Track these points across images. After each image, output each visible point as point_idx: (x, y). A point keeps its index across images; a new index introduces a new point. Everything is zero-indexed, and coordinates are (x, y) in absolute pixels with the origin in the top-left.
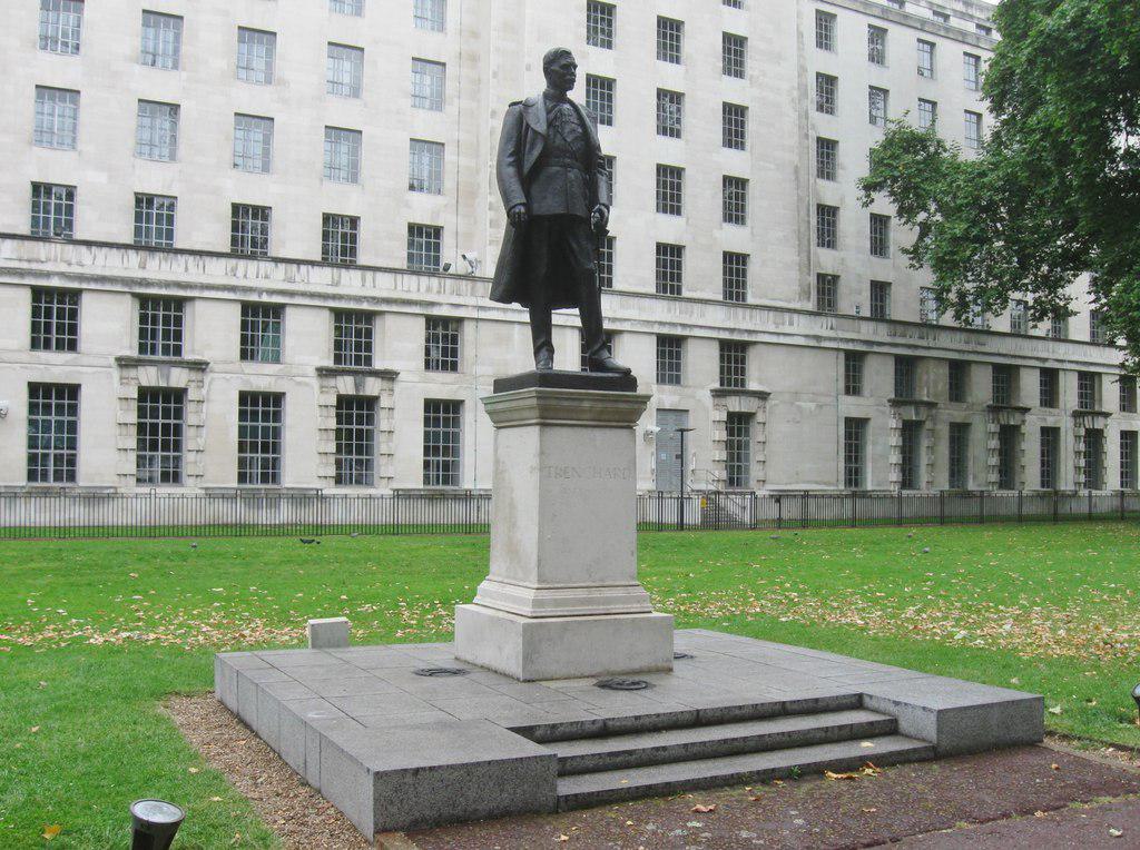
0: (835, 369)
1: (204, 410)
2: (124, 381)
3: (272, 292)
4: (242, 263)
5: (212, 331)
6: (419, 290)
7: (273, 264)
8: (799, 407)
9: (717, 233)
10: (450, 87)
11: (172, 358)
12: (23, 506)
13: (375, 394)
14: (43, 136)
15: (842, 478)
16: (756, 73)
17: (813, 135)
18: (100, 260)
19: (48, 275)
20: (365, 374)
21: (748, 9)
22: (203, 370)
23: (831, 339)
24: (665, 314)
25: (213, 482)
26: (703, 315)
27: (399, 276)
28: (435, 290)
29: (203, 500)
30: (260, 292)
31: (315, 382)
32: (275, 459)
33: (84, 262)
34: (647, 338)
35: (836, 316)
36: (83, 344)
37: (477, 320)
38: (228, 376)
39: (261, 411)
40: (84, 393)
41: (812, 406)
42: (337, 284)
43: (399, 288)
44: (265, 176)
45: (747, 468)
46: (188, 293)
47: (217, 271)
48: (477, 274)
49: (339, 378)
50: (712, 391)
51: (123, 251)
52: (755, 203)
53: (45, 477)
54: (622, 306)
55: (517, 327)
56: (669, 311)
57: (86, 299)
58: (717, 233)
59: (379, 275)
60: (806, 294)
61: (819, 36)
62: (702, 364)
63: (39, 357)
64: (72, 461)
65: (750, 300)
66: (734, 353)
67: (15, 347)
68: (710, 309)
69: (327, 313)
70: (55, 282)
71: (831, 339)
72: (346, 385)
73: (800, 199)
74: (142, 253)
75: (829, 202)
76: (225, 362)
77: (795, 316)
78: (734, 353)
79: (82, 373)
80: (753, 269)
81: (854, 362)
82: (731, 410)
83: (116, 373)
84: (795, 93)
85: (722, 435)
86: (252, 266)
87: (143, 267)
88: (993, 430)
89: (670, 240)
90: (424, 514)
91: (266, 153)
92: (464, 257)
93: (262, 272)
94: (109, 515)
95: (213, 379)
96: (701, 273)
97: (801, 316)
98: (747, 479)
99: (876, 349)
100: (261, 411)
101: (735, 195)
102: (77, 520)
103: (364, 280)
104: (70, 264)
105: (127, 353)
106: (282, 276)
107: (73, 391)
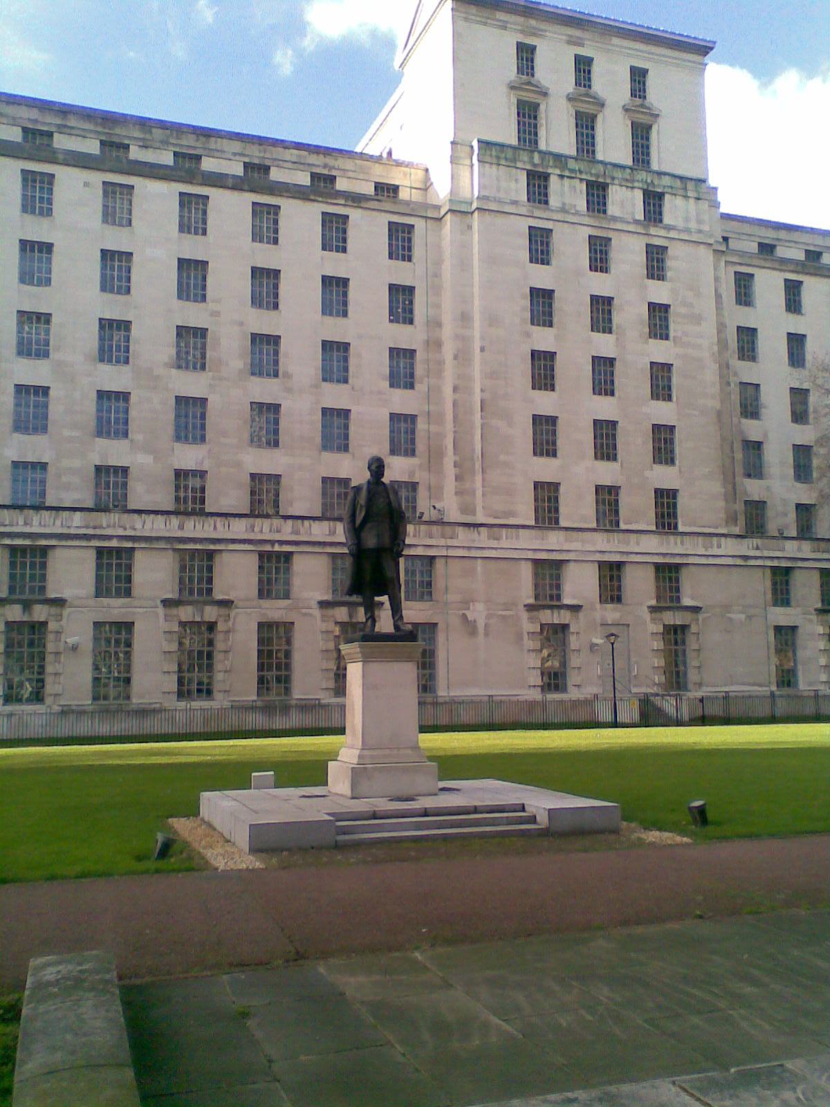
0: (761, 585)
3: (281, 543)
4: (258, 521)
5: (236, 575)
8: (730, 619)
9: (647, 473)
10: (419, 370)
11: (675, 604)
13: (567, 622)
14: (21, 426)
15: (774, 679)
16: (679, 334)
17: (734, 381)
18: (148, 525)
19: (110, 538)
20: (205, 603)
21: (671, 280)
23: (756, 558)
24: (607, 546)
26: (719, 546)
29: (33, 717)
30: (272, 542)
31: (317, 612)
34: (590, 565)
35: (768, 537)
36: (136, 591)
39: (116, 638)
40: (137, 628)
41: (743, 617)
44: (276, 450)
45: (685, 674)
46: (218, 547)
47: (239, 528)
48: (445, 520)
49: (8, 607)
50: (649, 607)
51: (165, 516)
52: (681, 447)
54: (566, 540)
55: (479, 561)
56: (608, 541)
57: (139, 557)
58: (647, 473)
60: (732, 519)
61: (738, 295)
62: (640, 586)
65: (681, 528)
66: (668, 574)
68: (644, 537)
70: (114, 543)
71: (756, 558)
72: (186, 613)
73: (723, 439)
74: (180, 517)
75: (754, 437)
77: (723, 539)
78: (668, 574)
80: (682, 502)
81: (781, 578)
82: (667, 623)
83: (161, 611)
84: (716, 348)
85: (658, 644)
86: (266, 524)
87: (181, 527)
88: (822, 632)
89: (607, 482)
92: (434, 507)
93: (274, 527)
96: (637, 508)
97: (729, 539)
98: (686, 683)
99: (800, 564)
100: (116, 638)
101: (663, 443)
104: (125, 529)
105: (169, 596)
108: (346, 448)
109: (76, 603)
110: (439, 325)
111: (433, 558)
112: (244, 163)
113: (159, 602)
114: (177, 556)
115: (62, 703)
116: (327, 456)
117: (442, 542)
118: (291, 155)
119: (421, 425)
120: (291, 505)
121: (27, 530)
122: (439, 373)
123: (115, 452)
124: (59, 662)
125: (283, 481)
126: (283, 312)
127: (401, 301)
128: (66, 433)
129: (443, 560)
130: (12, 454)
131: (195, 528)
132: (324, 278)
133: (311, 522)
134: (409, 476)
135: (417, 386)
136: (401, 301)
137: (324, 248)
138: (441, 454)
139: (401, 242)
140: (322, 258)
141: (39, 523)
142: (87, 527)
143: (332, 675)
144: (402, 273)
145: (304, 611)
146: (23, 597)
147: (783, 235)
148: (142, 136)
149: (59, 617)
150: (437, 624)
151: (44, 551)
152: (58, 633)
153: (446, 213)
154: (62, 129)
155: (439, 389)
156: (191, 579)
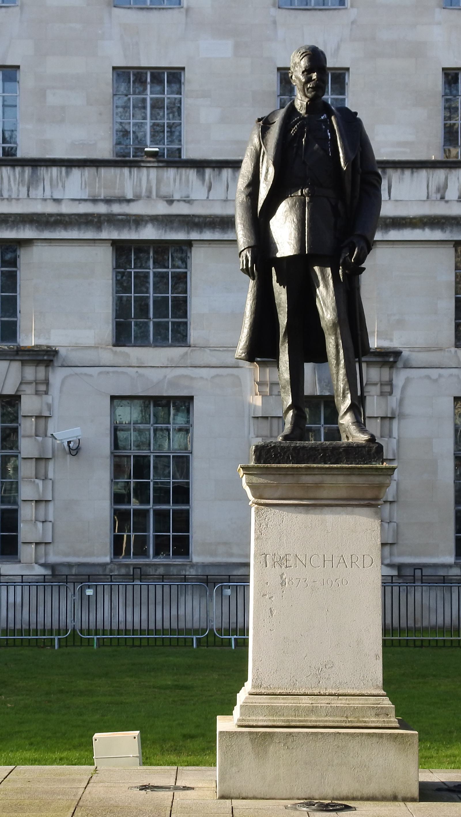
1: (395, 434)
19: (138, 221)
25: (411, 555)
33: (193, 197)
36: (194, 334)
38: (434, 373)
53: (141, 550)
63: (127, 355)
64: (183, 521)
67: (91, 342)
70: (149, 233)
76: (428, 349)
79: (192, 378)
95: (408, 380)
102: (189, 618)
104: (170, 202)
107: (185, 403)
109: (75, 357)
115: (53, 559)
142: (94, 201)
149: (43, 387)
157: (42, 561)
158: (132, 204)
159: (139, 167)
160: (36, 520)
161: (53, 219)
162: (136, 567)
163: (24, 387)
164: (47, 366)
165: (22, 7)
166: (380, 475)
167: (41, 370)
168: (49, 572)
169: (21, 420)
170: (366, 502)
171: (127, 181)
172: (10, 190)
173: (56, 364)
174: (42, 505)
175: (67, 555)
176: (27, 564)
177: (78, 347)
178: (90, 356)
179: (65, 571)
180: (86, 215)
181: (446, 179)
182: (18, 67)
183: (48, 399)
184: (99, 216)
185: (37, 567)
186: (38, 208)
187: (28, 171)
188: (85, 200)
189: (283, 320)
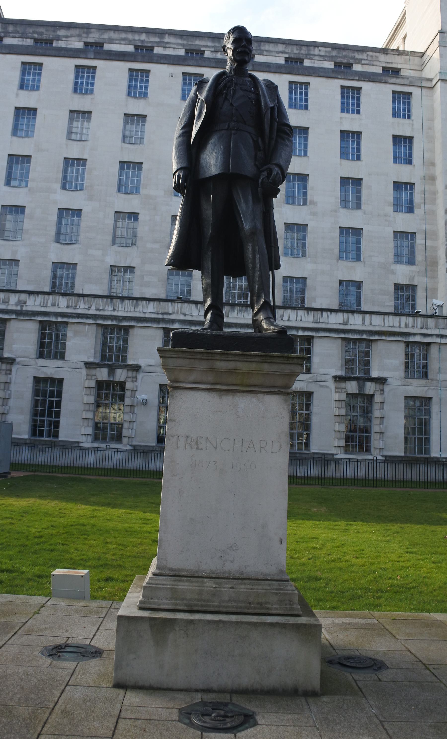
2: (90, 377)
6: (296, 320)
7: (306, 312)
10: (418, 198)
12: (18, 450)
13: (371, 393)
19: (173, 321)
22: (384, 384)
27: (387, 317)
28: (410, 325)
31: (332, 386)
32: (367, 437)
33: (193, 314)
37: (440, 344)
42: (346, 324)
43: (387, 324)
44: (304, 259)
49: (98, 369)
53: (41, 435)
59: (373, 316)
67: (154, 364)
69: (340, 341)
72: (103, 374)
83: (84, 372)
90: (404, 472)
91: (359, 249)
93: (299, 318)
94: (331, 471)
103: (363, 319)
104: (185, 315)
105: (92, 360)
106: (65, 304)
108: (359, 258)
109: (147, 369)
110: (433, 164)
111: (429, 344)
112: (285, 58)
113: (82, 364)
114: (100, 331)
115: (135, 443)
116: (343, 264)
117: (436, 332)
118: (320, 51)
119: (419, 240)
120: (315, 302)
121: (115, 313)
122: (434, 201)
123: (355, 272)
124: (133, 413)
125: (309, 282)
126: (310, 157)
127: (403, 146)
128: (149, 246)
129: (437, 347)
130: (111, 260)
131: (356, 322)
132: (342, 132)
133: (350, 315)
134: (409, 280)
135: (416, 211)
136: (403, 146)
137: (342, 111)
138: (435, 263)
139: (402, 104)
140: (341, 118)
141: (124, 310)
142: (158, 313)
143: (343, 436)
144: (403, 128)
145: (322, 383)
146: (110, 363)
147: (304, 51)
148: (213, 45)
149: (134, 380)
150: (432, 397)
151: (127, 329)
152: (382, 403)
153: (437, 82)
154: (159, 44)
155: (433, 213)
156: (57, 347)
157: (130, 444)
158: (171, 315)
159: (175, 302)
160: (129, 428)
161: (142, 319)
162: (52, 442)
163: (127, 379)
164: (137, 372)
165: (138, 247)
166: (291, 364)
167: (135, 373)
168: (132, 448)
169: (126, 391)
170: (277, 390)
171: (170, 307)
172: (128, 308)
173: (140, 371)
174: (132, 423)
175: (139, 442)
176: (125, 445)
177: (148, 365)
178: (152, 369)
179: (138, 448)
180: (154, 318)
181: (284, 313)
182: (135, 267)
183: (137, 384)
184: (159, 319)
185: (128, 446)
186: (137, 315)
187: (135, 301)
188: (154, 313)
189: (209, 231)
